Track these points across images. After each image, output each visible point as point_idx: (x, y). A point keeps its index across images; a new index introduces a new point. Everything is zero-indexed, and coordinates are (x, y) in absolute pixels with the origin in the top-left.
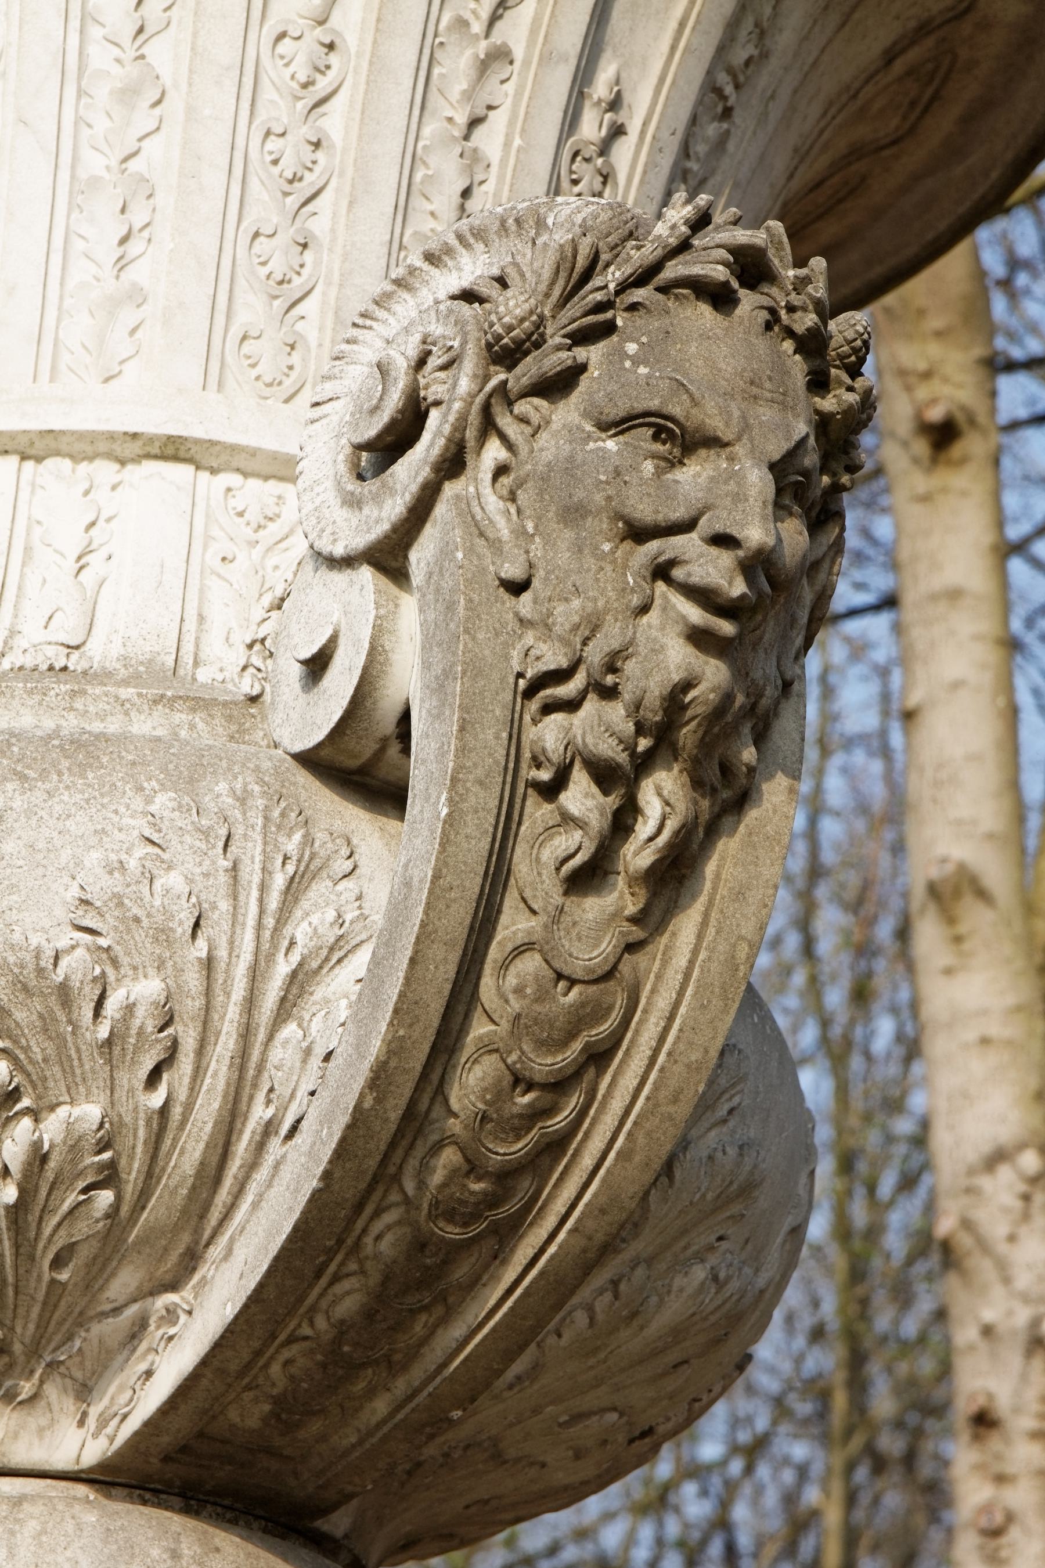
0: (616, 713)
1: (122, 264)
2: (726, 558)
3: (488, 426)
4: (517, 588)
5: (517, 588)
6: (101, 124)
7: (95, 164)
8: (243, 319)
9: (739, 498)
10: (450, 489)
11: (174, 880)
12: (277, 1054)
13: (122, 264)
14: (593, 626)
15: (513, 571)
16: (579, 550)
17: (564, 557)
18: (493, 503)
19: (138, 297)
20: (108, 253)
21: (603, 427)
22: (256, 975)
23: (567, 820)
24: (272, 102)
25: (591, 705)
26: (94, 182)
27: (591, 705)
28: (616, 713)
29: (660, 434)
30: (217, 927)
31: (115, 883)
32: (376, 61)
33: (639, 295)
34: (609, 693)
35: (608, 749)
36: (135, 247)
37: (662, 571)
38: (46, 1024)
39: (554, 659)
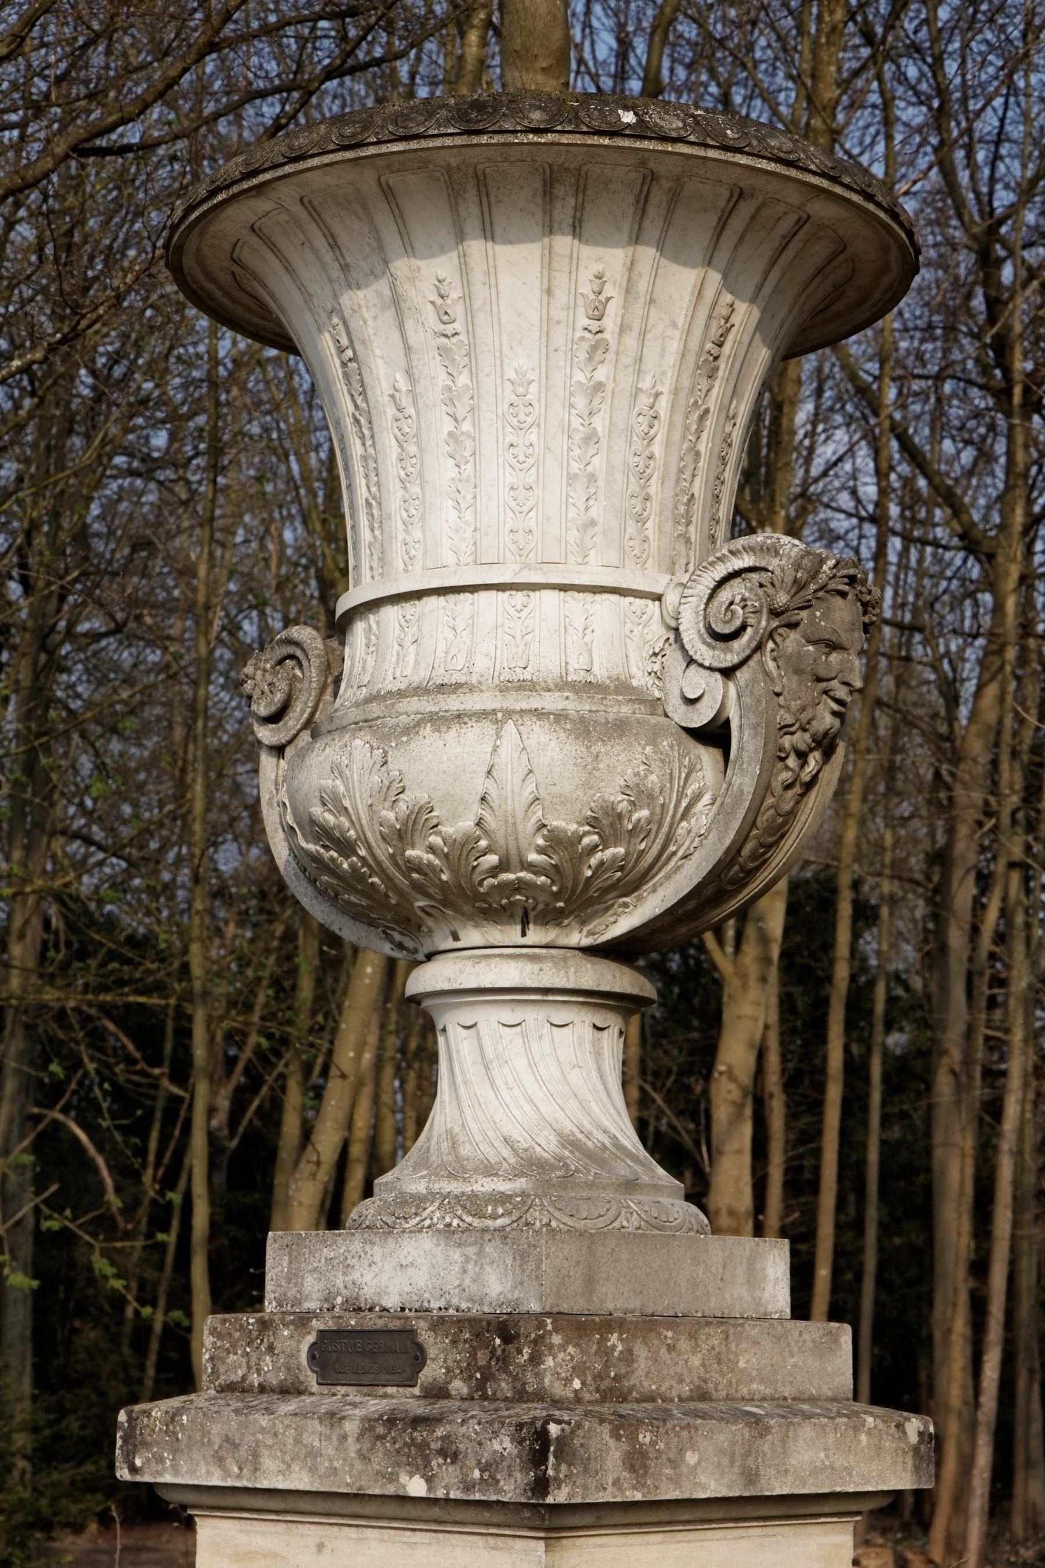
0: (807, 736)
1: (587, 509)
2: (846, 689)
3: (771, 636)
4: (778, 695)
5: (778, 695)
6: (578, 451)
7: (575, 467)
8: (629, 531)
9: (851, 670)
10: (757, 657)
11: (653, 778)
12: (679, 831)
13: (587, 509)
14: (803, 709)
15: (778, 689)
16: (800, 683)
17: (794, 685)
18: (771, 665)
19: (593, 523)
20: (581, 504)
21: (810, 642)
22: (676, 807)
23: (787, 768)
24: (833, 646)
25: (799, 734)
26: (576, 475)
27: (799, 734)
28: (807, 736)
29: (827, 645)
30: (666, 794)
31: (636, 780)
32: (671, 424)
33: (821, 594)
34: (804, 730)
35: (802, 747)
36: (591, 502)
37: (826, 692)
38: (612, 825)
39: (790, 720)
